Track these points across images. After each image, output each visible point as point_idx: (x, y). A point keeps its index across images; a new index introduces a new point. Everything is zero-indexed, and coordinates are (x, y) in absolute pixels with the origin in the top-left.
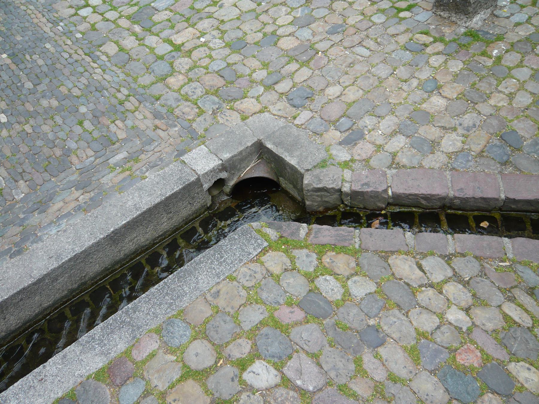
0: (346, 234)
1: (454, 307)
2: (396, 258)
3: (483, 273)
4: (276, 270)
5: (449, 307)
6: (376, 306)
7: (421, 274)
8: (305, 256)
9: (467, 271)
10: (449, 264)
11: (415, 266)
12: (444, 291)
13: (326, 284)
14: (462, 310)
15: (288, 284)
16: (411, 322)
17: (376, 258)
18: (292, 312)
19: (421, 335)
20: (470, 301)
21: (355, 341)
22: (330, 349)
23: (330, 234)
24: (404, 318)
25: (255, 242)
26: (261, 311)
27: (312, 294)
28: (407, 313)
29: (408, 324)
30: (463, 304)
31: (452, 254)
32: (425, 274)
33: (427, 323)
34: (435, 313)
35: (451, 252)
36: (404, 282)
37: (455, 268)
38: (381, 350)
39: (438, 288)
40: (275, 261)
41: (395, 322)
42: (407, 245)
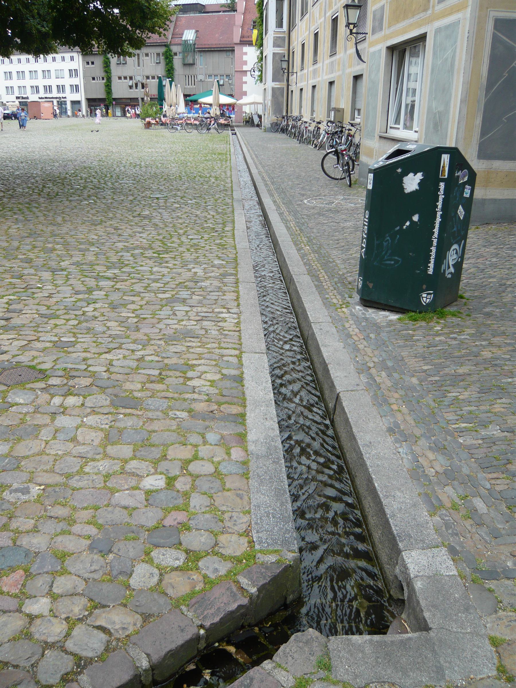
0: (206, 613)
1: (46, 613)
2: (135, 624)
3: (31, 672)
4: (223, 539)
5: (51, 611)
6: (116, 567)
7: (98, 623)
8: (218, 567)
9: (51, 660)
10: (75, 655)
11: (109, 627)
12: (64, 622)
13: (173, 555)
14: (36, 617)
15: (202, 536)
16: (79, 576)
17: (154, 610)
18: (175, 520)
19: (64, 572)
20: (33, 629)
21: (112, 535)
22: (126, 520)
23: (220, 600)
24: (86, 575)
25: (267, 543)
26: (198, 508)
27: (176, 541)
28: (87, 582)
29: (81, 573)
30: (38, 622)
31: (80, 673)
32: (94, 627)
33: (63, 584)
34: (62, 596)
35: (82, 675)
36: (109, 607)
37: (66, 656)
38: (88, 542)
39: (72, 623)
40: (234, 545)
41: (91, 566)
42: (134, 644)
